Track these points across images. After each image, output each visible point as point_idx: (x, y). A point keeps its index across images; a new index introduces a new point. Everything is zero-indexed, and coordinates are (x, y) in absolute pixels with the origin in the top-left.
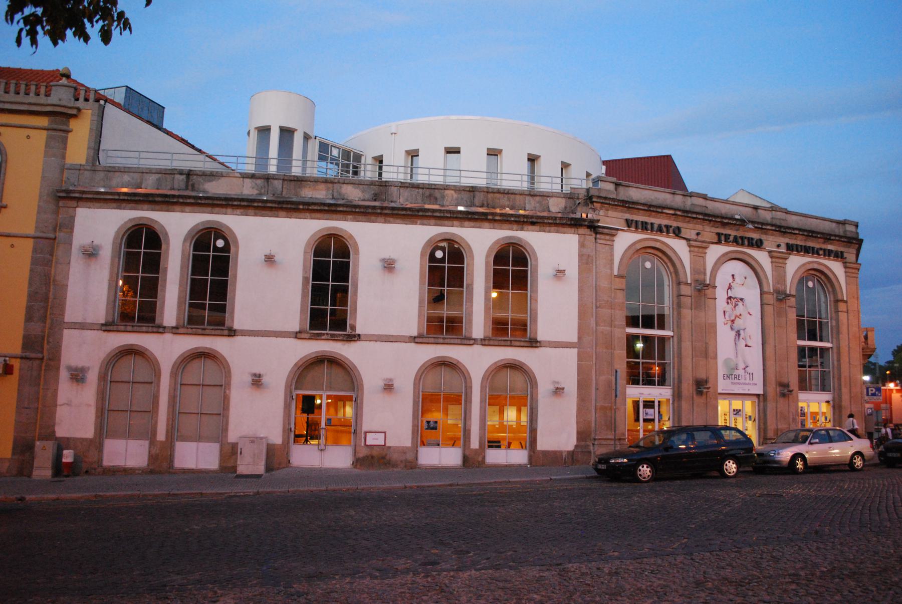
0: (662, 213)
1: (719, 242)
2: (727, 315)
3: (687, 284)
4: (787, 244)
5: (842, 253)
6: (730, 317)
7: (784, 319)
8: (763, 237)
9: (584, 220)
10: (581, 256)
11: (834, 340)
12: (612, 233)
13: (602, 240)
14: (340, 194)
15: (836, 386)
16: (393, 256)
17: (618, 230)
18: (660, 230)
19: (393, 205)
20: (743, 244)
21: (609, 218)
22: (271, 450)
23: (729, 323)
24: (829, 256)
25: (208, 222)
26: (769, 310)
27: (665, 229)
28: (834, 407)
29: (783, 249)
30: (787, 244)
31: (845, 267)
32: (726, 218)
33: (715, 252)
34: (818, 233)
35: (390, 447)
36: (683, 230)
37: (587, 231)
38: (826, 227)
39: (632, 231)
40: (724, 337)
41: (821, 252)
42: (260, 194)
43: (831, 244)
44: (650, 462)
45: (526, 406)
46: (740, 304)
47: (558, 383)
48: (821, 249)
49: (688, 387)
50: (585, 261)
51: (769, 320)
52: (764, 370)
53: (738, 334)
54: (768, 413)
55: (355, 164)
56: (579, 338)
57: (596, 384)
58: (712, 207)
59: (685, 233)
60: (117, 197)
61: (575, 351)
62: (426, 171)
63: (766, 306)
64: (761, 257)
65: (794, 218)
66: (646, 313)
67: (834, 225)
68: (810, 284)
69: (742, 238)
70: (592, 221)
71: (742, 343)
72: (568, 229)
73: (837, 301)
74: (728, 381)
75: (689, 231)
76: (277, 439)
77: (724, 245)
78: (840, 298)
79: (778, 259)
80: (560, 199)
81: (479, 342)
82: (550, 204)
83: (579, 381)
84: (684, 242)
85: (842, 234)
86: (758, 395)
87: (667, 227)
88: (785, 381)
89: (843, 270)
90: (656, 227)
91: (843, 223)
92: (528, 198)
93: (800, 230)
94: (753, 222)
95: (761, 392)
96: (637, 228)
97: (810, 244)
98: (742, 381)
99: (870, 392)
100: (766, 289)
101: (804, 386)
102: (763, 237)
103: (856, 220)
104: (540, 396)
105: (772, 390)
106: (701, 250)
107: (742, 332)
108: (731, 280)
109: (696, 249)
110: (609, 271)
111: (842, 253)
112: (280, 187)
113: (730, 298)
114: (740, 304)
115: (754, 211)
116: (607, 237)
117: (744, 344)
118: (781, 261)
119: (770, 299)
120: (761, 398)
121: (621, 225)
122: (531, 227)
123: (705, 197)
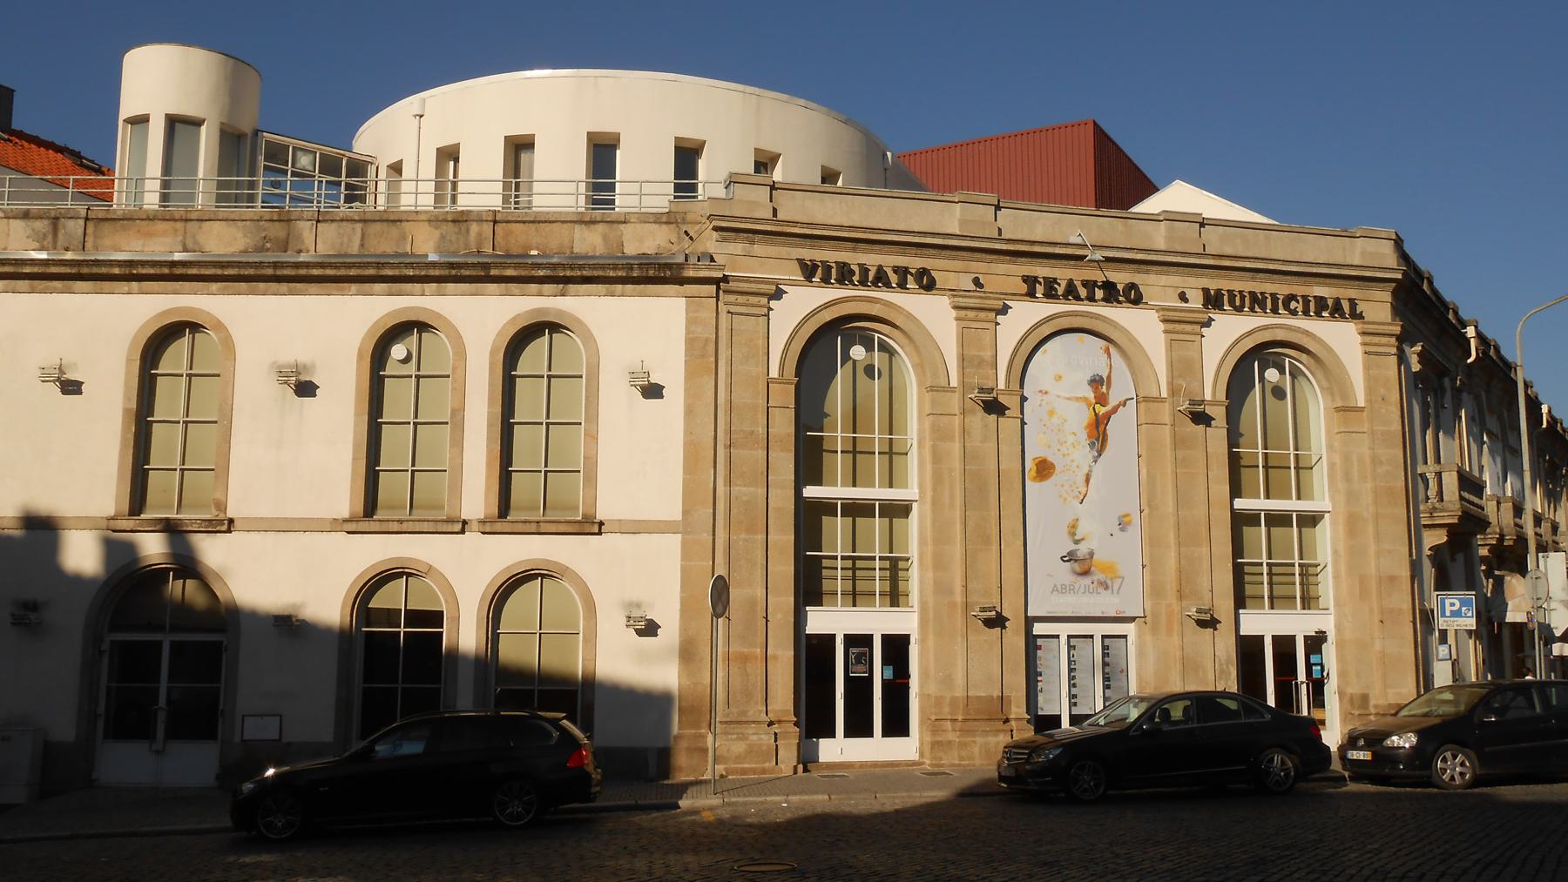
1: (1031, 294)
5: (1352, 302)
14: (196, 242)
16: (303, 358)
18: (881, 279)
19: (303, 258)
20: (1091, 298)
22: (50, 753)
25: (539, 311)
27: (894, 278)
29: (1196, 301)
30: (1206, 291)
33: (1026, 315)
35: (289, 744)
42: (260, 249)
47: (638, 605)
50: (705, 355)
55: (352, 180)
56: (685, 513)
60: (166, 271)
62: (635, 188)
69: (1085, 284)
75: (948, 271)
76: (64, 728)
81: (475, 526)
83: (684, 602)
99: (1448, 609)
102: (1138, 279)
109: (971, 314)
112: (80, 231)
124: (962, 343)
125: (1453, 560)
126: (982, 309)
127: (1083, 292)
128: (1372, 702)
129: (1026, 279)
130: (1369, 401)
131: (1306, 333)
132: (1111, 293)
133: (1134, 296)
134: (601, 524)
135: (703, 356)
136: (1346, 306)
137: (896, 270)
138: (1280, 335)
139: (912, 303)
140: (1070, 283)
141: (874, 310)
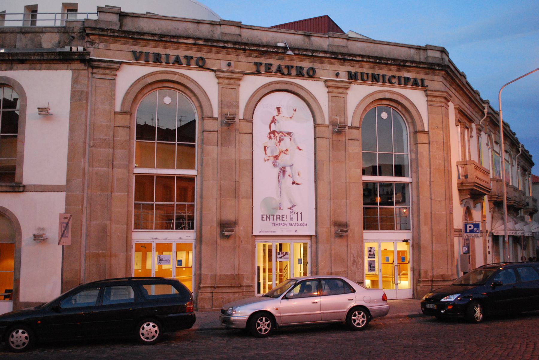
0: (178, 43)
1: (258, 73)
2: (268, 151)
3: (212, 118)
5: (422, 80)
6: (272, 152)
7: (343, 153)
8: (317, 66)
9: (74, 54)
10: (73, 93)
11: (414, 175)
12: (114, 67)
13: (99, 74)
15: (415, 223)
17: (120, 63)
18: (178, 61)
20: (289, 75)
21: (115, 52)
23: (272, 159)
24: (406, 84)
26: (324, 143)
27: (183, 61)
28: (413, 246)
29: (343, 77)
30: (349, 73)
31: (427, 96)
32: (263, 46)
33: (250, 85)
34: (388, 59)
37: (81, 66)
38: (402, 54)
39: (141, 65)
40: (264, 177)
41: (394, 81)
43: (408, 71)
44: (26, 325)
45: (191, 250)
46: (287, 138)
48: (394, 77)
49: (211, 229)
50: (79, 98)
51: (323, 155)
52: (316, 209)
53: (283, 170)
54: (319, 256)
56: (68, 181)
57: (88, 229)
58: (246, 35)
59: (209, 64)
61: (62, 195)
63: (317, 139)
64: (316, 89)
65: (359, 44)
66: (397, 164)
67: (413, 51)
68: (384, 115)
69: (287, 67)
70: (80, 54)
71: (288, 181)
72: (61, 66)
73: (416, 132)
74: (268, 223)
77: (264, 75)
78: (419, 128)
79: (337, 89)
80: (54, 35)
82: (43, 40)
84: (212, 74)
85: (422, 60)
86: (310, 236)
87: (189, 58)
88: (342, 219)
89: (425, 99)
90: (172, 59)
91: (425, 49)
92: (18, 36)
93: (363, 56)
94: (292, 49)
95: (313, 233)
96: (147, 61)
97: (380, 71)
98: (289, 221)
99: (468, 229)
100: (319, 121)
101: (370, 224)
102: (204, 55)
103: (441, 45)
104: (23, 244)
105: (327, 228)
106: (232, 81)
107: (288, 169)
108: (275, 113)
109: (226, 81)
110: (108, 108)
111: (422, 80)
113: (273, 132)
114: (287, 138)
115: (306, 39)
116: (108, 72)
117: (290, 180)
118: (340, 90)
119: (327, 132)
120: (313, 237)
122: (20, 66)
123: (238, 25)
125: (475, 207)
127: (286, 71)
129: (256, 64)
131: (189, 78)
132: (300, 74)
133: (311, 75)
134: (24, 186)
135: (80, 100)
136: (419, 82)
137: (186, 57)
139: (196, 75)
140: (178, 57)
141: (175, 78)
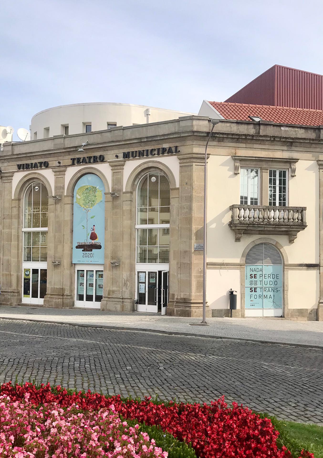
1: (73, 164)
4: (124, 153)
20: (90, 162)
24: (163, 153)
33: (71, 172)
36: (50, 163)
39: (21, 171)
52: (73, 222)
75: (53, 162)
79: (117, 167)
109: (58, 173)
111: (176, 147)
118: (119, 167)
121: (15, 168)
124: (56, 182)
126: (60, 171)
128: (176, 297)
130: (181, 185)
133: (102, 159)
136: (173, 149)
138: (150, 165)
